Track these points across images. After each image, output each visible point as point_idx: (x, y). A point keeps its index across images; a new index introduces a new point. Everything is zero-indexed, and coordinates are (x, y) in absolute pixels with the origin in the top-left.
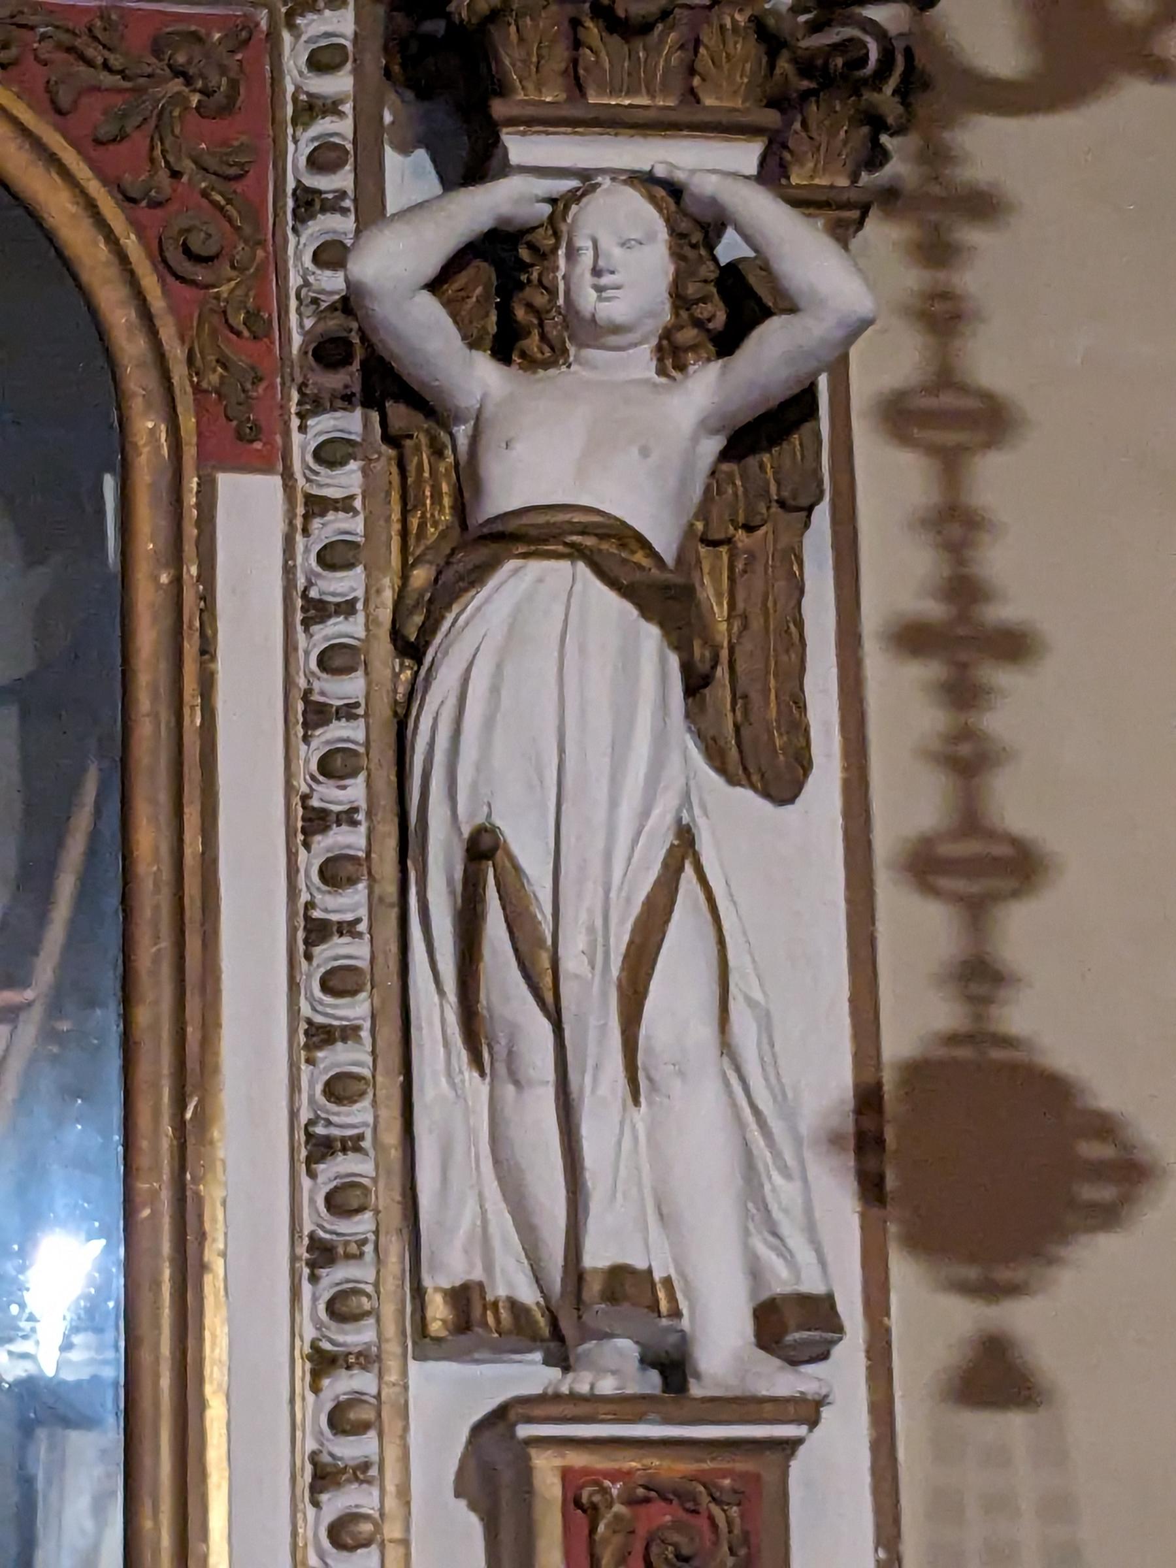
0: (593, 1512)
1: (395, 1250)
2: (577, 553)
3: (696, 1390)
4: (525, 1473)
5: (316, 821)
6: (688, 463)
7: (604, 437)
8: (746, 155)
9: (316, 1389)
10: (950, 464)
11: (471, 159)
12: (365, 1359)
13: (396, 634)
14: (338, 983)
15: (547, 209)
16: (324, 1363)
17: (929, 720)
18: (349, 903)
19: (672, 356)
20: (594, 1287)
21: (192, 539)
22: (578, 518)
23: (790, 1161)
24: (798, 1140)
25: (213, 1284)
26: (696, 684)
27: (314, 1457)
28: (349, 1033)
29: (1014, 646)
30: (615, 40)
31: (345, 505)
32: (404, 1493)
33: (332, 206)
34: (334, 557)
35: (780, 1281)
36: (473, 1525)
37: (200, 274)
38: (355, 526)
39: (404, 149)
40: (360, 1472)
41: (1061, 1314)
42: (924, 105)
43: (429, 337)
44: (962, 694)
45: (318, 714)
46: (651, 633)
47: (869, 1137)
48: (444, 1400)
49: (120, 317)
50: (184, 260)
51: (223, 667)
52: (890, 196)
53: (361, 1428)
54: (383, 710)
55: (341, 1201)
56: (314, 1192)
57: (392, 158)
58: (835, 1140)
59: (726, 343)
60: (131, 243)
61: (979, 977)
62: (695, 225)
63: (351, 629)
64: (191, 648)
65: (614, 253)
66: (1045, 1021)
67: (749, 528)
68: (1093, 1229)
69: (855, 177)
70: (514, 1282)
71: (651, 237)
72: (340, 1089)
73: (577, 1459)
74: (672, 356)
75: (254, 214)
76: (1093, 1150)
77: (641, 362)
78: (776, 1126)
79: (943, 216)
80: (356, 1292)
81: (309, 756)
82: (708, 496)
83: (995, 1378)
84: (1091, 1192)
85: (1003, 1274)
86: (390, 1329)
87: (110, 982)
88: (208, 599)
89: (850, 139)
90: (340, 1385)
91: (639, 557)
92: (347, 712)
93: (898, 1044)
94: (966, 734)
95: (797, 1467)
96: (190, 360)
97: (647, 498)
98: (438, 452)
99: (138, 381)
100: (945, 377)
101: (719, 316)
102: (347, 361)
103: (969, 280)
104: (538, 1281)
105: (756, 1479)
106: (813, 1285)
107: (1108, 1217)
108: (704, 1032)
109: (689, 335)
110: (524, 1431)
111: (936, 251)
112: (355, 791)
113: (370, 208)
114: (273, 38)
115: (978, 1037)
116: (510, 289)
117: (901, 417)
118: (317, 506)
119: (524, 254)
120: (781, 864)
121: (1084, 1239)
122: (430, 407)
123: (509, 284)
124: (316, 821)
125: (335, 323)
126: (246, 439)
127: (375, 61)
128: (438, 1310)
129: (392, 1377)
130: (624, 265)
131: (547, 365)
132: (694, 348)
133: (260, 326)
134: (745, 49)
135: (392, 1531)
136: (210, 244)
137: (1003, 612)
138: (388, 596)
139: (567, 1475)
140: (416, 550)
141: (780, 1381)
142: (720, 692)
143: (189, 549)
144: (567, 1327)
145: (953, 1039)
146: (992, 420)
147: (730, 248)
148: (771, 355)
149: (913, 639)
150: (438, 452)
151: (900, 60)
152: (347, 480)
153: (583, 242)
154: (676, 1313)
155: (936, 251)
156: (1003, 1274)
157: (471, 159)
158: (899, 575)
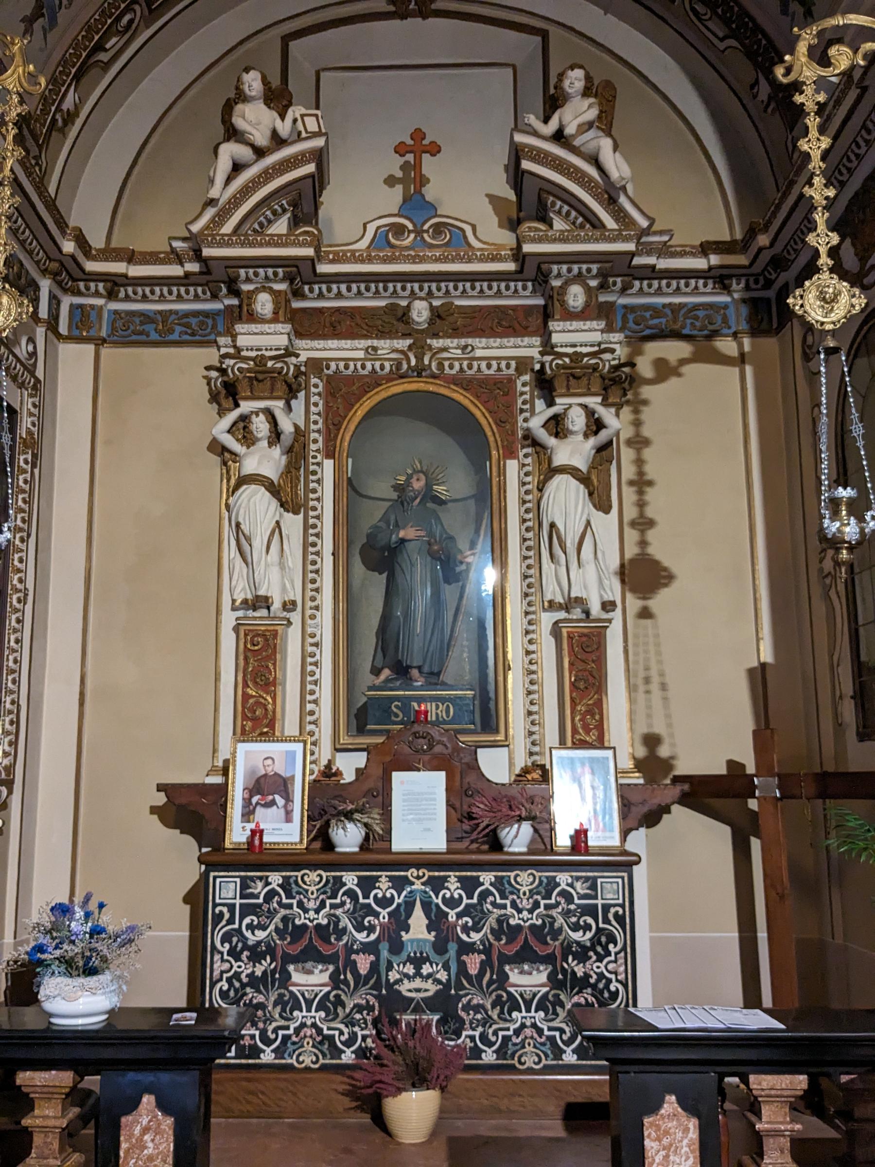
1: (539, 595)
5: (524, 521)
7: (573, 452)
8: (599, 399)
10: (639, 451)
12: (534, 613)
14: (528, 549)
16: (527, 613)
17: (634, 498)
18: (530, 535)
19: (586, 436)
21: (502, 472)
25: (508, 601)
26: (591, 494)
28: (530, 557)
29: (650, 483)
33: (526, 411)
34: (527, 474)
35: (606, 598)
36: (553, 640)
40: (533, 632)
41: (659, 602)
42: (634, 385)
43: (542, 435)
44: (641, 493)
45: (524, 502)
46: (582, 486)
47: (623, 573)
48: (547, 619)
49: (489, 433)
50: (500, 423)
51: (508, 494)
55: (529, 586)
56: (525, 584)
57: (537, 401)
58: (616, 573)
59: (596, 433)
60: (490, 420)
62: (590, 413)
63: (529, 487)
65: (575, 418)
66: (656, 551)
70: (559, 599)
72: (529, 567)
74: (586, 436)
76: (663, 574)
77: (580, 437)
79: (639, 404)
81: (523, 528)
83: (645, 614)
84: (663, 581)
87: (489, 549)
88: (505, 483)
90: (530, 617)
92: (529, 501)
93: (628, 555)
95: (608, 631)
97: (581, 463)
100: (638, 435)
101: (594, 428)
106: (612, 599)
107: (666, 585)
108: (592, 556)
111: (636, 412)
112: (531, 516)
113: (533, 412)
116: (557, 425)
117: (629, 443)
118: (524, 465)
120: (606, 526)
123: (557, 424)
124: (524, 521)
126: (511, 453)
127: (534, 384)
128: (546, 604)
130: (577, 420)
133: (514, 433)
134: (599, 380)
136: (505, 418)
141: (605, 616)
142: (596, 495)
145: (638, 555)
146: (646, 442)
147: (596, 416)
148: (603, 436)
149: (631, 483)
152: (529, 460)
155: (636, 412)
157: (550, 403)
158: (629, 471)
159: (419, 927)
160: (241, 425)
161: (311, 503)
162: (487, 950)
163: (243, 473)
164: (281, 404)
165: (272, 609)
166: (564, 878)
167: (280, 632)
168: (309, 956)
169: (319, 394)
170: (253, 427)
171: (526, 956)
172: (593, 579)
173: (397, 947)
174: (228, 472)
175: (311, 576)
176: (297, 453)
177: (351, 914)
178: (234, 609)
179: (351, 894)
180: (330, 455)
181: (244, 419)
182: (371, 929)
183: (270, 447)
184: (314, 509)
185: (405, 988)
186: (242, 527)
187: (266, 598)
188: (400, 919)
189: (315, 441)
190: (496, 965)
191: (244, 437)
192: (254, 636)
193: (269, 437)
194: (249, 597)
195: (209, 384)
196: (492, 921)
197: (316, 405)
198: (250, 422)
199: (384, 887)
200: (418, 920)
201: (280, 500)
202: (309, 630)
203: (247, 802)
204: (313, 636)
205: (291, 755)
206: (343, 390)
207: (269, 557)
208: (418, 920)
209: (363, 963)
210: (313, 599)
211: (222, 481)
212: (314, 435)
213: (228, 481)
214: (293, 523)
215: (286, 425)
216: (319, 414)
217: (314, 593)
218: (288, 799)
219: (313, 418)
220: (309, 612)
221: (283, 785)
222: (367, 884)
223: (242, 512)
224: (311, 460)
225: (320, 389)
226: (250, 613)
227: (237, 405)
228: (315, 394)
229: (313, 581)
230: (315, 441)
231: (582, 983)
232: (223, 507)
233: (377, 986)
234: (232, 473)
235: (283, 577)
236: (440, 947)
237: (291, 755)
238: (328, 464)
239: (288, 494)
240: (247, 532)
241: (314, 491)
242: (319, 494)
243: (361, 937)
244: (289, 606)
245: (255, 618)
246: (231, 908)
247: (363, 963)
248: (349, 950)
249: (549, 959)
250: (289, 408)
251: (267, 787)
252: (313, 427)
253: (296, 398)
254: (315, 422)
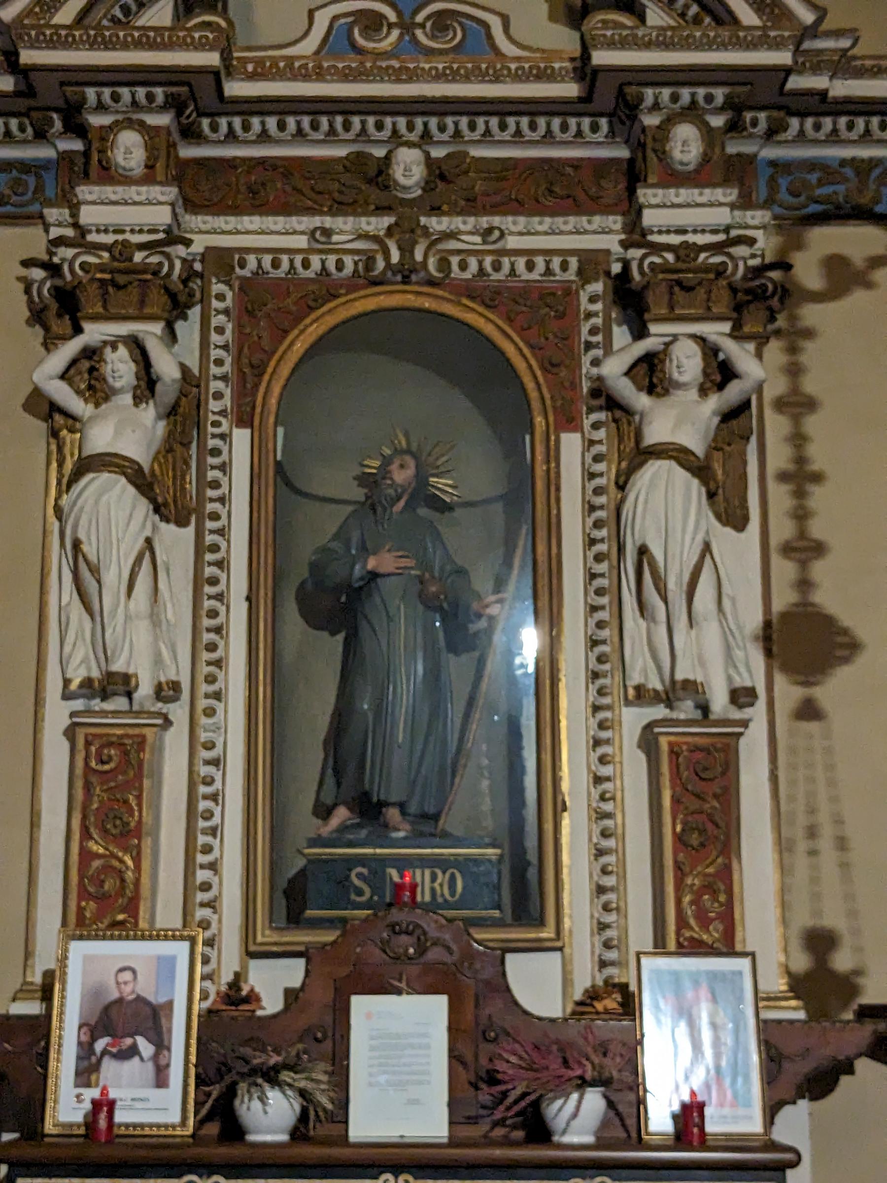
0: (678, 755)
2: (670, 457)
3: (712, 717)
4: (657, 742)
5: (592, 542)
6: (708, 429)
8: (726, 327)
9: (594, 716)
10: (796, 420)
11: (640, 333)
12: (609, 708)
13: (617, 483)
14: (600, 592)
15: (662, 347)
16: (596, 708)
18: (603, 567)
19: (703, 392)
20: (678, 686)
21: (553, 455)
22: (671, 447)
23: (741, 644)
24: (743, 638)
25: (562, 685)
27: (594, 738)
28: (602, 608)
29: (817, 478)
30: (683, 293)
31: (600, 442)
32: (621, 748)
33: (596, 346)
34: (597, 459)
35: (738, 682)
37: (555, 370)
38: (603, 449)
39: (619, 325)
40: (608, 742)
41: (835, 689)
44: (800, 494)
45: (592, 508)
46: (695, 482)
47: (768, 637)
48: (633, 719)
49: (530, 385)
50: (550, 366)
52: (778, 333)
53: (607, 728)
54: (612, 506)
59: (721, 387)
60: (533, 362)
61: (804, 584)
62: (710, 350)
64: (553, 489)
65: (684, 361)
66: (826, 598)
67: (729, 444)
68: (840, 665)
69: (765, 327)
71: (695, 355)
72: (600, 625)
73: (672, 738)
74: (703, 392)
75: (572, 350)
76: (840, 639)
77: (693, 394)
78: (737, 634)
79: (797, 337)
80: (606, 687)
81: (590, 522)
82: (716, 435)
83: (808, 711)
85: (812, 679)
86: (616, 699)
87: (529, 592)
88: (558, 474)
89: (763, 314)
90: (602, 715)
91: (692, 458)
92: (601, 507)
93: (778, 605)
94: (801, 507)
95: (742, 741)
96: (552, 398)
97: (694, 441)
98: (629, 423)
99: (536, 405)
101: (718, 378)
102: (601, 396)
103: (803, 358)
104: (662, 681)
105: (728, 745)
106: (748, 683)
108: (712, 606)
109: (708, 385)
110: (657, 730)
111: (793, 350)
112: (604, 532)
114: (577, 292)
115: (805, 604)
116: (651, 372)
117: (780, 405)
118: (592, 443)
119: (656, 361)
120: (739, 553)
121: (838, 668)
122: (628, 411)
124: (592, 542)
125: (595, 385)
126: (570, 422)
127: (610, 297)
128: (631, 692)
129: (617, 712)
130: (687, 363)
131: (663, 395)
132: (709, 389)
133: (574, 385)
134: (726, 294)
135: (617, 759)
136: (558, 360)
137: (815, 467)
138: (614, 471)
139: (670, 744)
140: (623, 455)
141: (736, 714)
142: (720, 498)
143: (552, 459)
144: (671, 695)
145: (796, 605)
147: (721, 356)
148: (734, 392)
149: (783, 477)
150: (629, 423)
151: (779, 290)
152: (601, 434)
153: (674, 357)
154: (704, 693)
155: (793, 350)
156: (812, 679)
157: (640, 333)
158: (779, 456)
160: (85, 364)
161: (210, 507)
163: (85, 454)
164: (157, 328)
165: (136, 696)
167: (150, 738)
169: (226, 312)
170: (107, 370)
174: (60, 449)
175: (207, 637)
176: (184, 416)
178: (67, 696)
180: (244, 419)
181: (91, 354)
183: (136, 405)
184: (215, 516)
186: (85, 548)
187: (126, 678)
189: (218, 396)
191: (90, 387)
192: (102, 747)
193: (136, 388)
194: (95, 674)
195: (27, 291)
197: (220, 330)
198: (102, 360)
201: (153, 500)
202: (203, 736)
203: (86, 1050)
204: (210, 746)
207: (132, 604)
210: (211, 679)
211: (48, 464)
212: (218, 385)
213: (61, 465)
214: (175, 542)
215: (166, 366)
216: (225, 347)
217: (212, 669)
218: (161, 1044)
219: (215, 353)
220: (202, 703)
221: (150, 1019)
223: (83, 522)
224: (211, 430)
225: (229, 302)
226: (97, 704)
227: (78, 330)
228: (218, 312)
229: (212, 647)
230: (218, 396)
232: (50, 511)
234: (67, 451)
235: (156, 639)
238: (241, 438)
239: (169, 490)
240: (92, 558)
241: (215, 484)
242: (225, 489)
244: (167, 691)
245: (104, 713)
250: (171, 336)
251: (124, 1022)
252: (214, 370)
253: (185, 318)
254: (219, 362)
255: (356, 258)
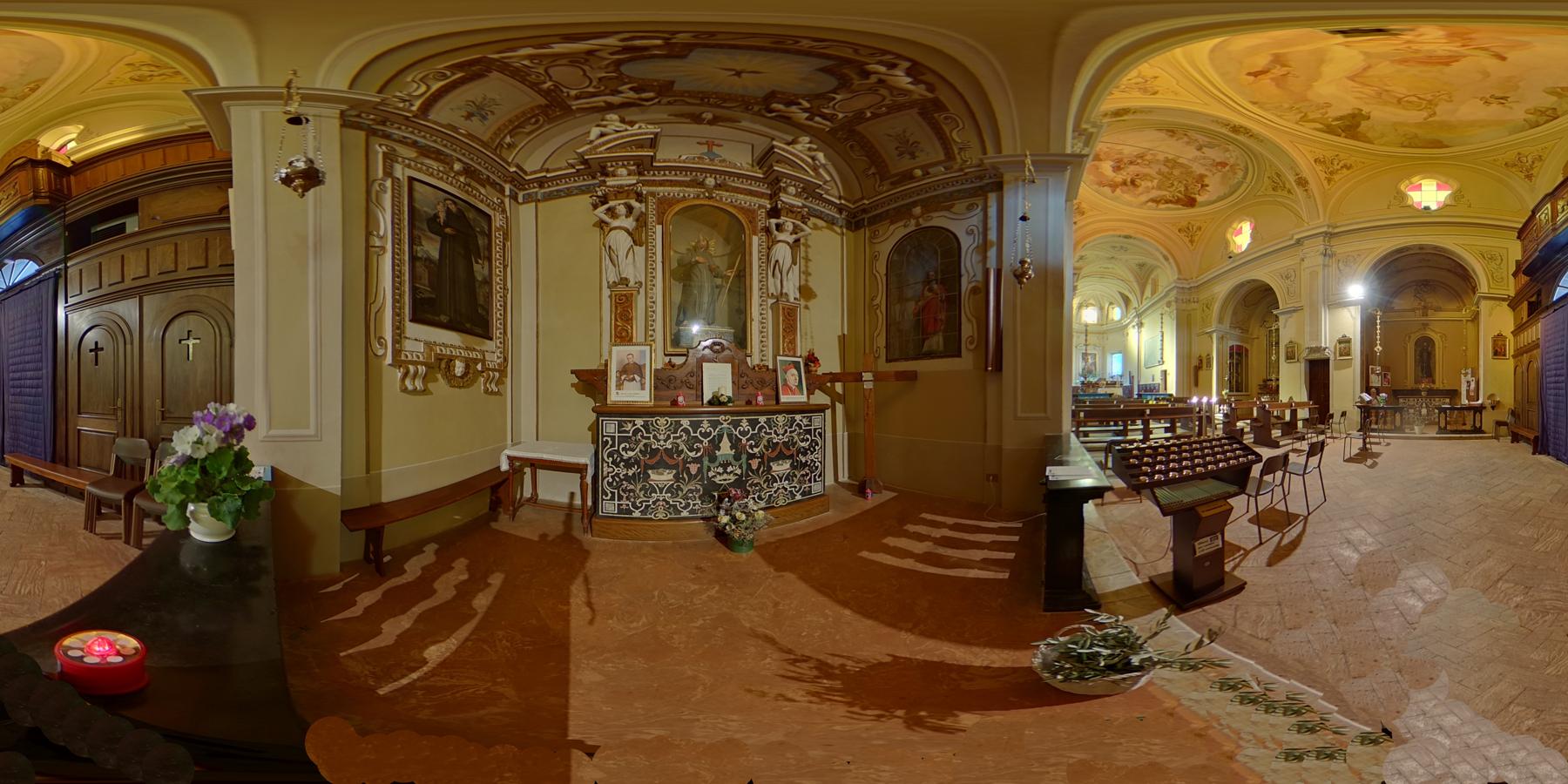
66: (811, 284)
136: (752, 221)
159: (725, 448)
162: (762, 457)
166: (798, 417)
168: (661, 465)
171: (781, 457)
172: (791, 290)
173: (713, 459)
176: (642, 220)
177: (686, 442)
179: (685, 430)
182: (698, 450)
185: (717, 480)
188: (715, 444)
190: (766, 462)
196: (764, 442)
199: (705, 427)
200: (725, 445)
203: (619, 379)
205: (643, 353)
206: (664, 204)
208: (725, 445)
209: (694, 468)
218: (642, 376)
221: (639, 369)
222: (695, 425)
231: (805, 465)
233: (702, 479)
236: (737, 457)
237: (643, 353)
238: (659, 228)
243: (692, 454)
246: (613, 438)
247: (694, 468)
248: (685, 462)
249: (791, 457)
251: (631, 371)
255: (344, 107)
